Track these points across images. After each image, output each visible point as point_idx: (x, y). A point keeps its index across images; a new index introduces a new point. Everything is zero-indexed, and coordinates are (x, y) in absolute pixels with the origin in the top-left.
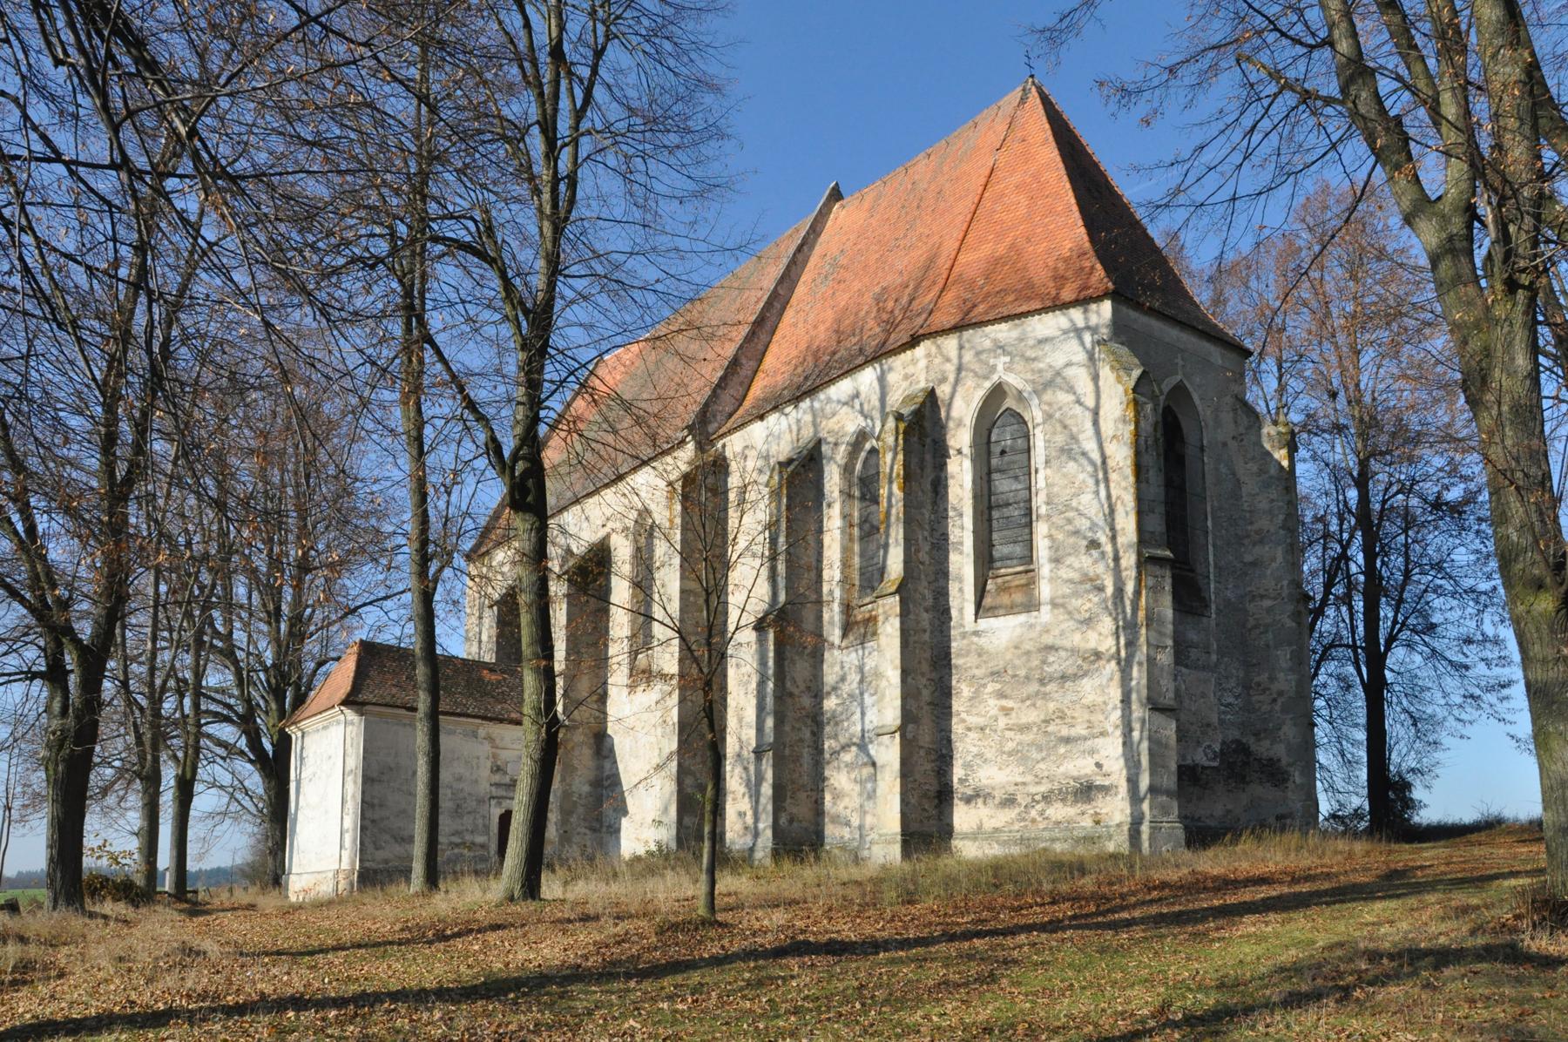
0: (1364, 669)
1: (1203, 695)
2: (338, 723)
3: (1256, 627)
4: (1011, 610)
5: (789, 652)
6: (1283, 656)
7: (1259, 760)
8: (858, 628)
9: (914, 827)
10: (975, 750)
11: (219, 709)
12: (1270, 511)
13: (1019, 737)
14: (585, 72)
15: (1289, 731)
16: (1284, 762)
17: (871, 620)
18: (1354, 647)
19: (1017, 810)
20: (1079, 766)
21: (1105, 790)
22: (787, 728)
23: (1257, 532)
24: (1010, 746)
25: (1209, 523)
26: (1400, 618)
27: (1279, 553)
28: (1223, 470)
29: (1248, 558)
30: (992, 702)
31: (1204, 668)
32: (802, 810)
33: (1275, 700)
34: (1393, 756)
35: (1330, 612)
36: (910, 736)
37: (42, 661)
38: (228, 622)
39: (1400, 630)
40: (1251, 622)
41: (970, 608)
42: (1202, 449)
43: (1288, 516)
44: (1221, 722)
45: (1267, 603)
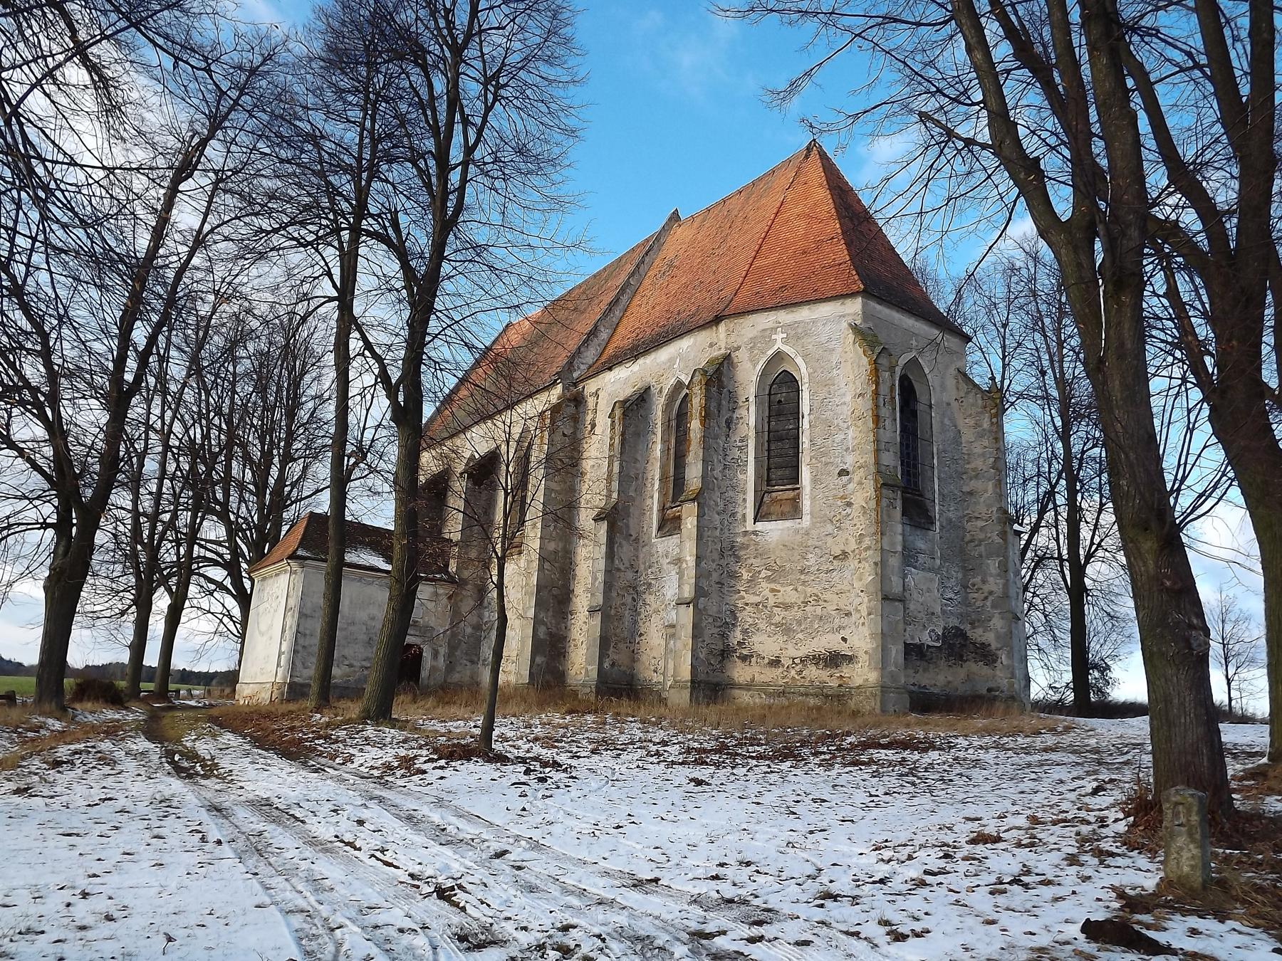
0: (1067, 573)
1: (929, 590)
2: (286, 571)
3: (972, 541)
4: (783, 517)
5: (618, 538)
6: (993, 565)
7: (974, 644)
8: (669, 525)
9: (702, 677)
10: (751, 621)
11: (215, 557)
12: (983, 455)
13: (783, 613)
14: (478, 121)
15: (997, 623)
16: (993, 647)
17: (678, 518)
18: (1060, 557)
19: (781, 670)
20: (827, 642)
21: (850, 659)
22: (614, 594)
23: (974, 470)
24: (777, 619)
25: (935, 461)
26: (1097, 540)
27: (990, 485)
28: (947, 422)
29: (966, 489)
30: (764, 584)
31: (930, 570)
32: (622, 658)
33: (986, 598)
34: (1092, 644)
35: (1043, 531)
36: (701, 606)
37: (55, 516)
38: (227, 494)
39: (1096, 550)
40: (968, 537)
41: (750, 512)
42: (931, 407)
43: (997, 459)
44: (943, 612)
45: (980, 523)
